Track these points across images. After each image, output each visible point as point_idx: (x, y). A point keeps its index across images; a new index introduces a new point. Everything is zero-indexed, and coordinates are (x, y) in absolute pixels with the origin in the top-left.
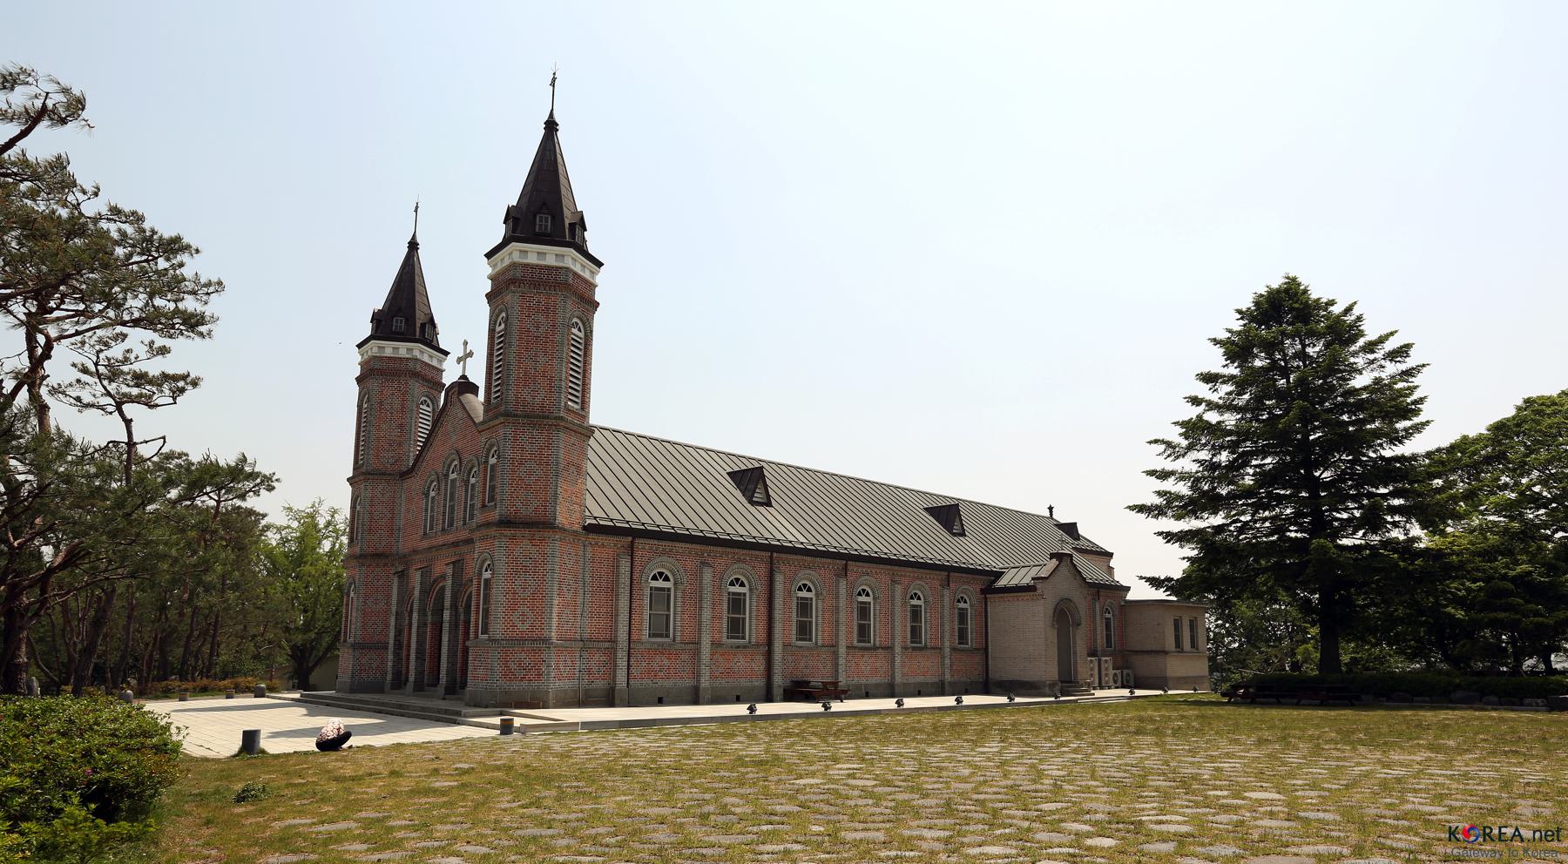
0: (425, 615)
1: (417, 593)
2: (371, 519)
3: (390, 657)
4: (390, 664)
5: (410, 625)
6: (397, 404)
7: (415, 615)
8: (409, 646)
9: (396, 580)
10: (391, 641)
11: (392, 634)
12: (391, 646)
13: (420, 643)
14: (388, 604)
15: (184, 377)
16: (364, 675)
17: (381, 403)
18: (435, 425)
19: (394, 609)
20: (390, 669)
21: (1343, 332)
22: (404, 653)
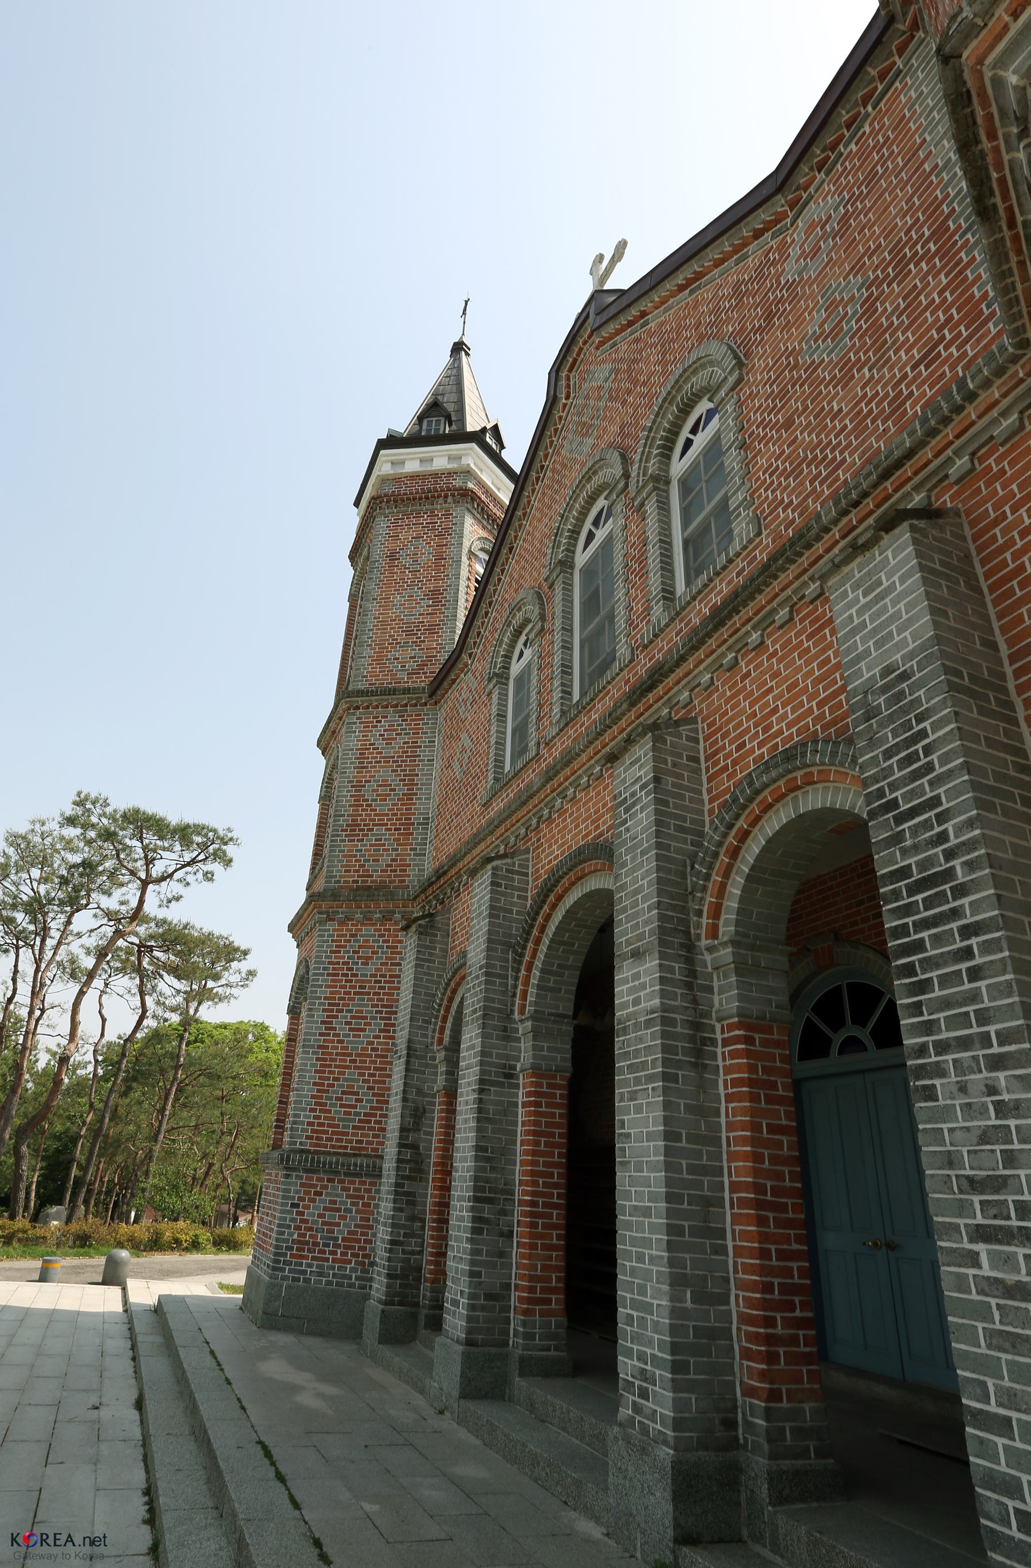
0: (507, 1034)
1: (476, 953)
2: (358, 800)
3: (386, 1207)
4: (383, 1234)
5: (451, 1094)
6: (426, 553)
7: (471, 1037)
8: (446, 1170)
9: (410, 943)
10: (391, 1150)
11: (393, 1123)
12: (389, 1166)
13: (490, 1155)
14: (388, 1029)
15: (184, 834)
16: (309, 1266)
17: (393, 556)
18: (490, 567)
19: (402, 1036)
20: (381, 1254)
21: (267, 1028)
22: (430, 1195)
